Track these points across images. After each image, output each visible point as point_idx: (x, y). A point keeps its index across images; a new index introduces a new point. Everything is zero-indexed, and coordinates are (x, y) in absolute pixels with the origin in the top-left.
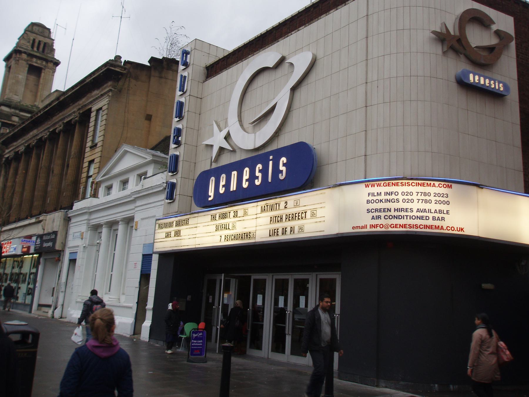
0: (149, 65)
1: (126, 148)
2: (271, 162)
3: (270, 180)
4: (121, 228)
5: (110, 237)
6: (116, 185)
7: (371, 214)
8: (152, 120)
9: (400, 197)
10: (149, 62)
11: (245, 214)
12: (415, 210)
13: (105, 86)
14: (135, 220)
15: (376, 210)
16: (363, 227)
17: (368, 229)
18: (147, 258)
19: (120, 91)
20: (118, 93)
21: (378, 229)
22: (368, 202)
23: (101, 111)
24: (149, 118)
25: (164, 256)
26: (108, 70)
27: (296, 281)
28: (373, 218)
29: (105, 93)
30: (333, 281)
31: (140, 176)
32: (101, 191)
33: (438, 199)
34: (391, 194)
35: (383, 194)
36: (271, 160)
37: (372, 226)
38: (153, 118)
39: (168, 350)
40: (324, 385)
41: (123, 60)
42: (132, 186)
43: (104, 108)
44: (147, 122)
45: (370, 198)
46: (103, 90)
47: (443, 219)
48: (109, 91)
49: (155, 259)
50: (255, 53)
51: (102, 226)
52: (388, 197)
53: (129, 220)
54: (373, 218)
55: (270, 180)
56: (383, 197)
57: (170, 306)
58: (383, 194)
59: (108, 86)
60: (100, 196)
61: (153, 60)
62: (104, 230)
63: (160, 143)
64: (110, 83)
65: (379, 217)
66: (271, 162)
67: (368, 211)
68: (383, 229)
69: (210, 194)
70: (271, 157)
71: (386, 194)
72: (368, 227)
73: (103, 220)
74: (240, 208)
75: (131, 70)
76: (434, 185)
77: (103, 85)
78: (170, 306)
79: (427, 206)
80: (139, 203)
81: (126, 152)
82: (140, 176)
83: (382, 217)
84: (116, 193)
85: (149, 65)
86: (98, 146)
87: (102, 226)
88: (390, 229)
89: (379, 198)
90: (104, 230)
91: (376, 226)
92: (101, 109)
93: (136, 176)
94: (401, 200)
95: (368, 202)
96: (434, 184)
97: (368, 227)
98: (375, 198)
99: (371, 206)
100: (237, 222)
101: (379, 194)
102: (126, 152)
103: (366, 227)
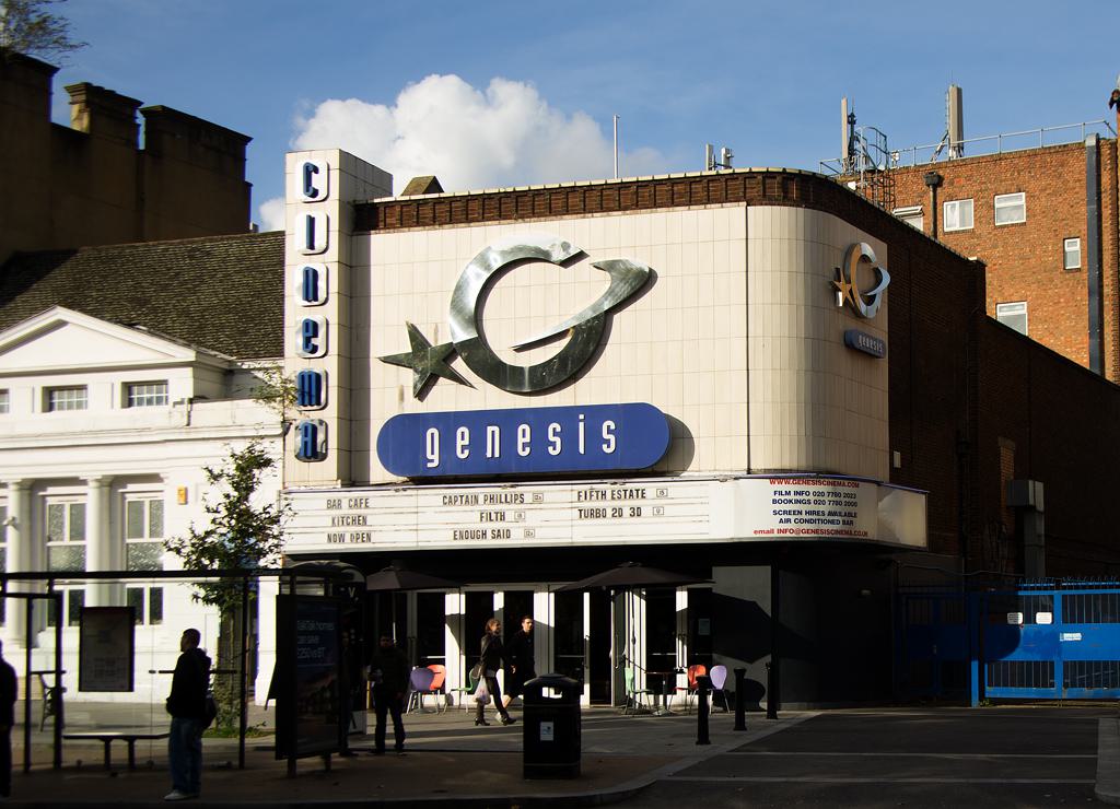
2: (581, 425)
3: (582, 451)
7: (778, 517)
9: (811, 497)
10: (96, 99)
11: (537, 499)
12: (826, 513)
15: (785, 512)
16: (768, 532)
17: (776, 535)
21: (788, 535)
22: (774, 501)
28: (781, 521)
33: (847, 500)
34: (801, 493)
35: (792, 493)
36: (581, 421)
37: (780, 531)
40: (819, 713)
45: (777, 497)
47: (852, 522)
50: (810, 407)
52: (798, 497)
54: (781, 521)
55: (582, 451)
56: (792, 497)
57: (865, 592)
58: (792, 493)
65: (788, 521)
66: (581, 425)
67: (775, 513)
68: (794, 535)
69: (429, 456)
70: (582, 417)
71: (796, 493)
72: (776, 531)
74: (528, 490)
76: (844, 485)
78: (865, 592)
79: (821, 508)
83: (792, 521)
88: (801, 535)
89: (788, 497)
91: (785, 531)
94: (812, 502)
95: (774, 501)
97: (776, 531)
98: (783, 498)
99: (778, 507)
100: (527, 512)
101: (788, 493)
103: (772, 531)
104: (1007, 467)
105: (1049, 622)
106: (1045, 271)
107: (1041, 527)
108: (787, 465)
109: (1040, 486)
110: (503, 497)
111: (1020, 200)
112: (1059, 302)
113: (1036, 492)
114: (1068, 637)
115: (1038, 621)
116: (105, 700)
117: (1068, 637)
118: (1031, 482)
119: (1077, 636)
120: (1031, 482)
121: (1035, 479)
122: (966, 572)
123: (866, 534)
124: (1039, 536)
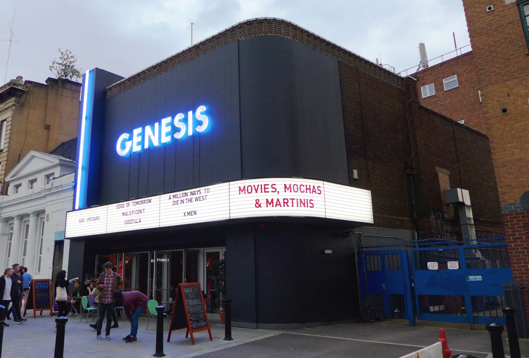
0: (46, 84)
1: (33, 153)
4: (32, 220)
5: (21, 228)
6: (25, 183)
8: (51, 129)
10: (46, 81)
13: (8, 101)
14: (46, 213)
18: (59, 244)
19: (22, 105)
20: (20, 106)
23: (5, 123)
24: (48, 128)
25: (74, 240)
26: (12, 88)
27: (188, 254)
29: (9, 107)
30: (148, 254)
31: (48, 176)
32: (11, 189)
38: (51, 127)
39: (468, 240)
41: (24, 80)
42: (40, 184)
43: (8, 120)
44: (46, 131)
46: (6, 104)
48: (12, 106)
49: (67, 245)
51: (13, 218)
53: (39, 214)
59: (12, 101)
60: (9, 193)
61: (49, 80)
62: (16, 222)
63: (57, 148)
64: (13, 99)
73: (14, 214)
75: (32, 89)
77: (7, 100)
78: (328, 252)
80: (49, 199)
81: (33, 157)
82: (48, 176)
84: (24, 191)
85: (46, 84)
86: (3, 151)
87: (13, 218)
90: (16, 222)
92: (5, 120)
93: (44, 176)
96: (66, 76)
102: (33, 157)
104: (444, 179)
105: (457, 268)
106: (471, 105)
107: (469, 214)
108: (155, 327)
109: (466, 193)
110: (295, 204)
111: (455, 77)
112: (480, 117)
113: (464, 196)
114: (472, 278)
115: (449, 268)
116: (331, 189)
117: (472, 278)
118: (459, 190)
119: (479, 278)
120: (459, 190)
121: (462, 188)
122: (418, 239)
123: (241, 190)
124: (469, 219)
